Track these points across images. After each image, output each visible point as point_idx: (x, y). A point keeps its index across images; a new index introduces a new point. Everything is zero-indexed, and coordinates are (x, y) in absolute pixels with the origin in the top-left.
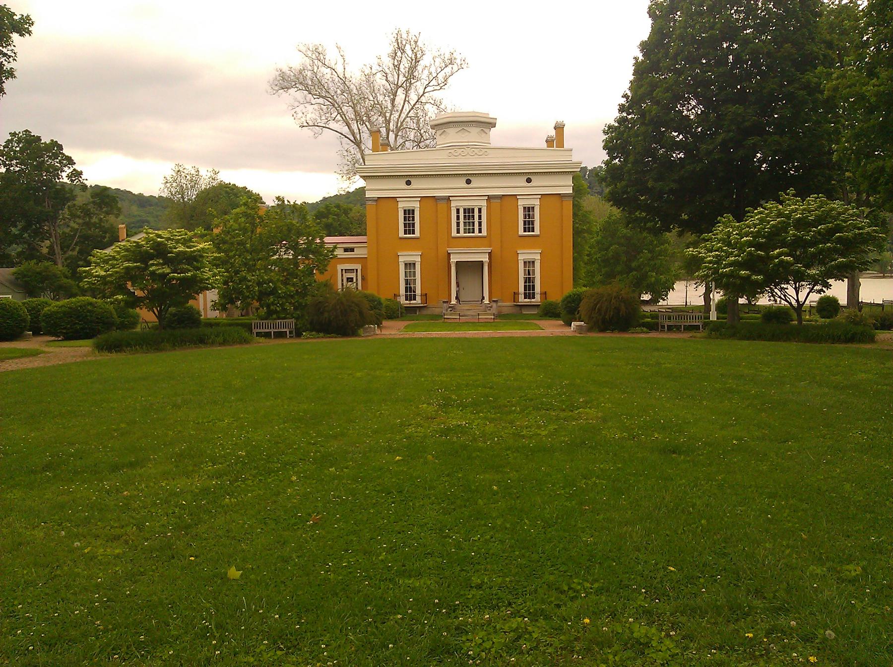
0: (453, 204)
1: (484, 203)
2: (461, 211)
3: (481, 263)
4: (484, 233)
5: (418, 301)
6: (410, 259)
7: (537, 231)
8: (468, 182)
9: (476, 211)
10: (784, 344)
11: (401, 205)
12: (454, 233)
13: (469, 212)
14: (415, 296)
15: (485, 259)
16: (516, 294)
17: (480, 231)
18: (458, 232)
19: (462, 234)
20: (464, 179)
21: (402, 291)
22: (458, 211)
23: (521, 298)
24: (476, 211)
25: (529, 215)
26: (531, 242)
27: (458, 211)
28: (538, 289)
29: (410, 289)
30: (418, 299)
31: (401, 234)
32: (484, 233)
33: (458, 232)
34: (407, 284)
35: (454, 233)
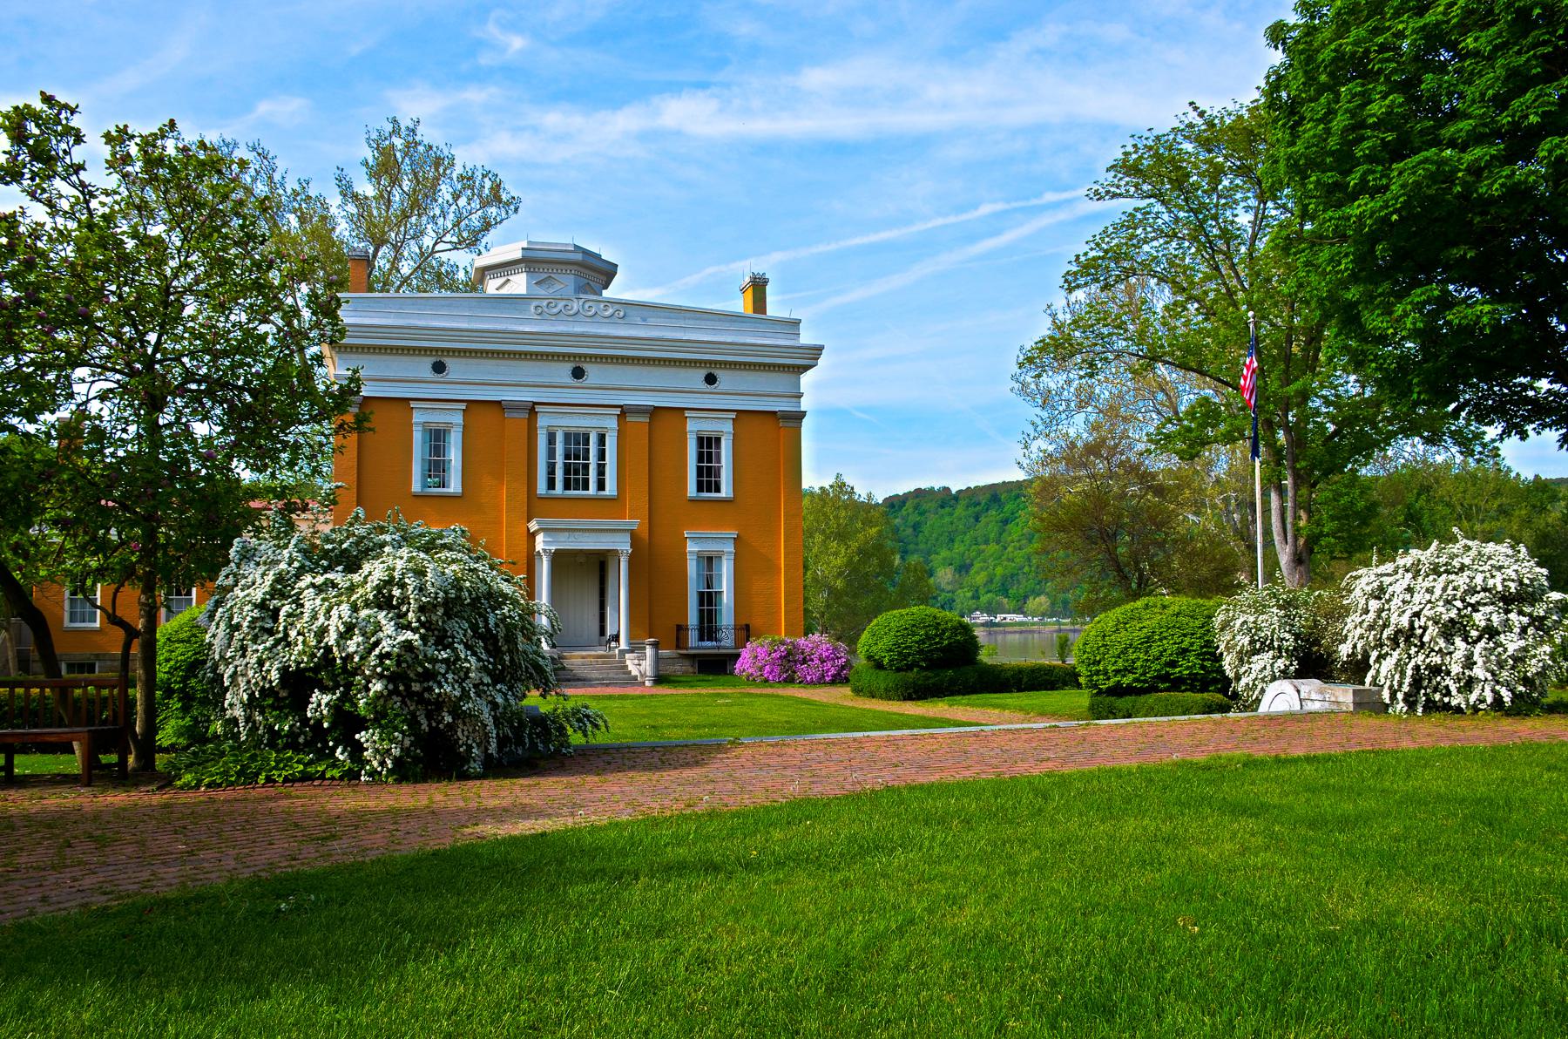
0: (543, 422)
1: (612, 424)
2: (559, 438)
4: (454, 486)
6: (711, 547)
7: (726, 491)
8: (439, 368)
10: (592, 779)
11: (417, 417)
12: (542, 488)
13: (577, 441)
15: (623, 545)
16: (681, 629)
17: (601, 485)
18: (551, 484)
20: (428, 362)
22: (551, 439)
23: (692, 638)
25: (709, 454)
26: (712, 511)
27: (551, 439)
31: (692, 490)
32: (611, 488)
33: (551, 484)
35: (542, 488)
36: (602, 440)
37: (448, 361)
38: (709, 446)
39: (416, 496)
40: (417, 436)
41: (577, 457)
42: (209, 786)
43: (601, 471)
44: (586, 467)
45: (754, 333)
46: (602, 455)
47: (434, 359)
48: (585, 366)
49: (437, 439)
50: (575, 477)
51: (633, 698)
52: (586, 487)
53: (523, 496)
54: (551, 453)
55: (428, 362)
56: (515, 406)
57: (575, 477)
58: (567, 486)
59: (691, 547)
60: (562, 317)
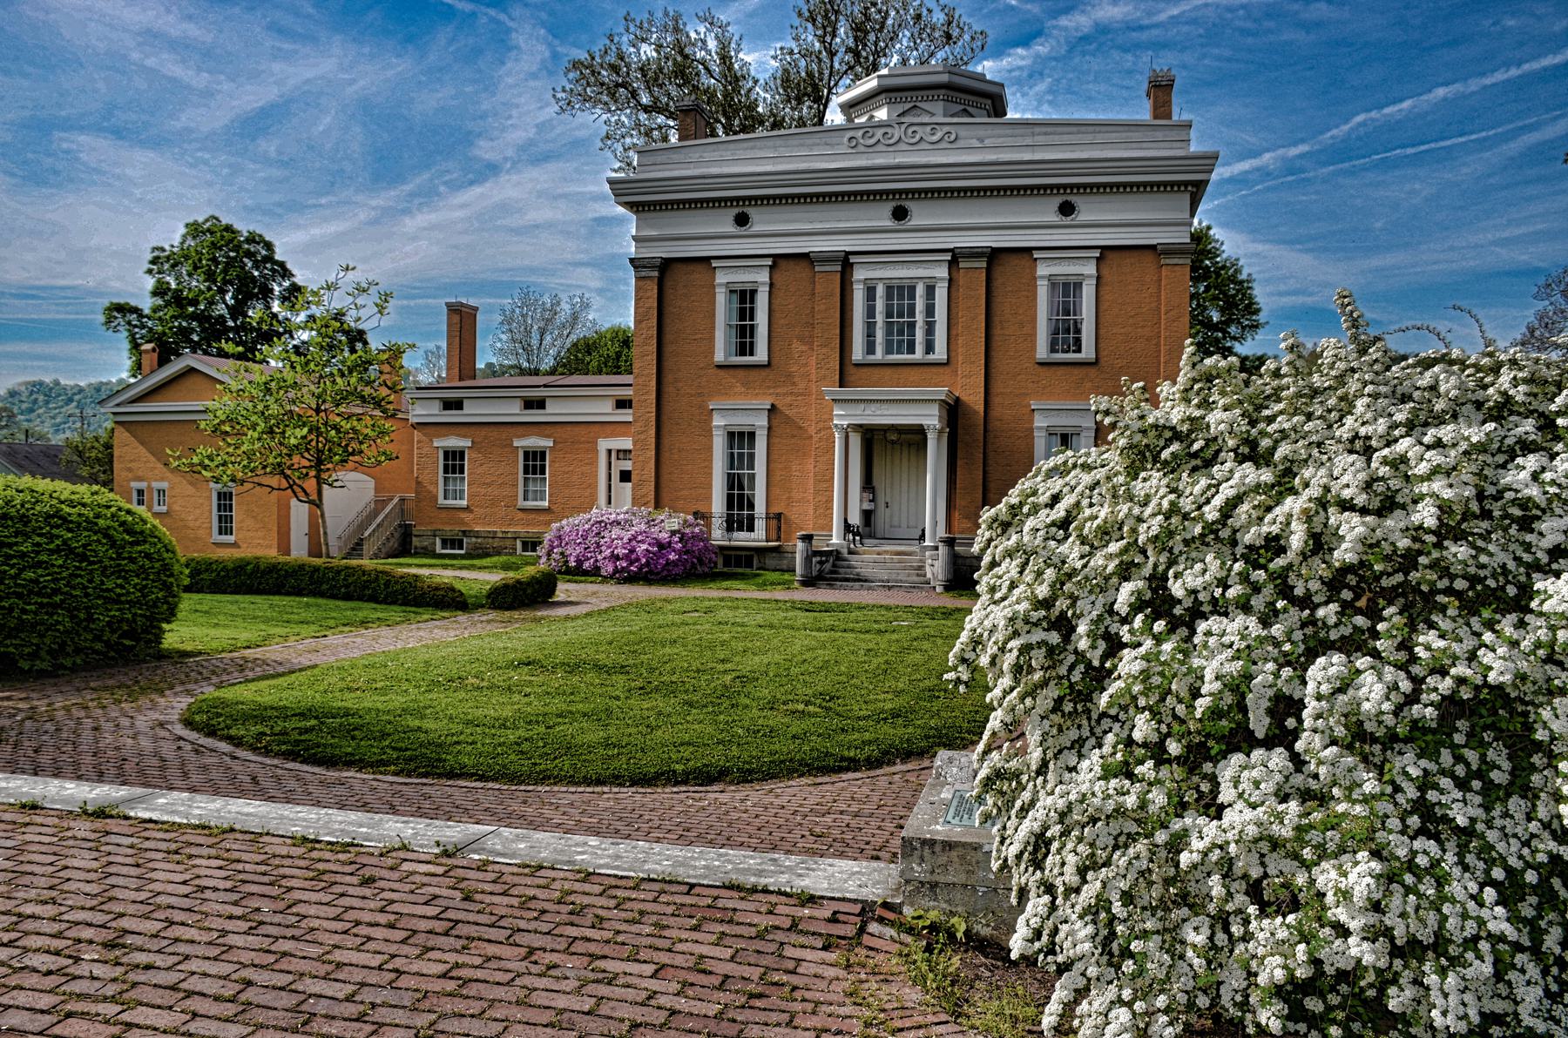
0: (859, 274)
1: (942, 272)
2: (880, 291)
3: (920, 431)
4: (940, 353)
5: (757, 537)
6: (741, 421)
8: (900, 214)
9: (920, 290)
11: (1043, 270)
13: (901, 292)
14: (751, 519)
15: (931, 418)
17: (929, 348)
18: (870, 348)
19: (879, 355)
20: (887, 208)
21: (718, 506)
22: (871, 293)
24: (920, 290)
27: (871, 293)
28: (760, 508)
29: (738, 499)
30: (760, 525)
31: (1042, 352)
32: (940, 353)
33: (870, 348)
34: (731, 487)
35: (858, 353)
36: (930, 291)
37: (910, 205)
38: (901, 297)
39: (720, 367)
40: (721, 298)
41: (901, 315)
42: (1056, 757)
43: (930, 329)
44: (912, 325)
45: (1127, 143)
46: (930, 311)
47: (736, 211)
48: (909, 204)
49: (742, 300)
50: (901, 335)
51: (576, 618)
52: (911, 350)
53: (835, 364)
54: (871, 312)
55: (887, 208)
56: (827, 258)
57: (901, 335)
58: (889, 351)
59: (1040, 422)
60: (880, 148)
